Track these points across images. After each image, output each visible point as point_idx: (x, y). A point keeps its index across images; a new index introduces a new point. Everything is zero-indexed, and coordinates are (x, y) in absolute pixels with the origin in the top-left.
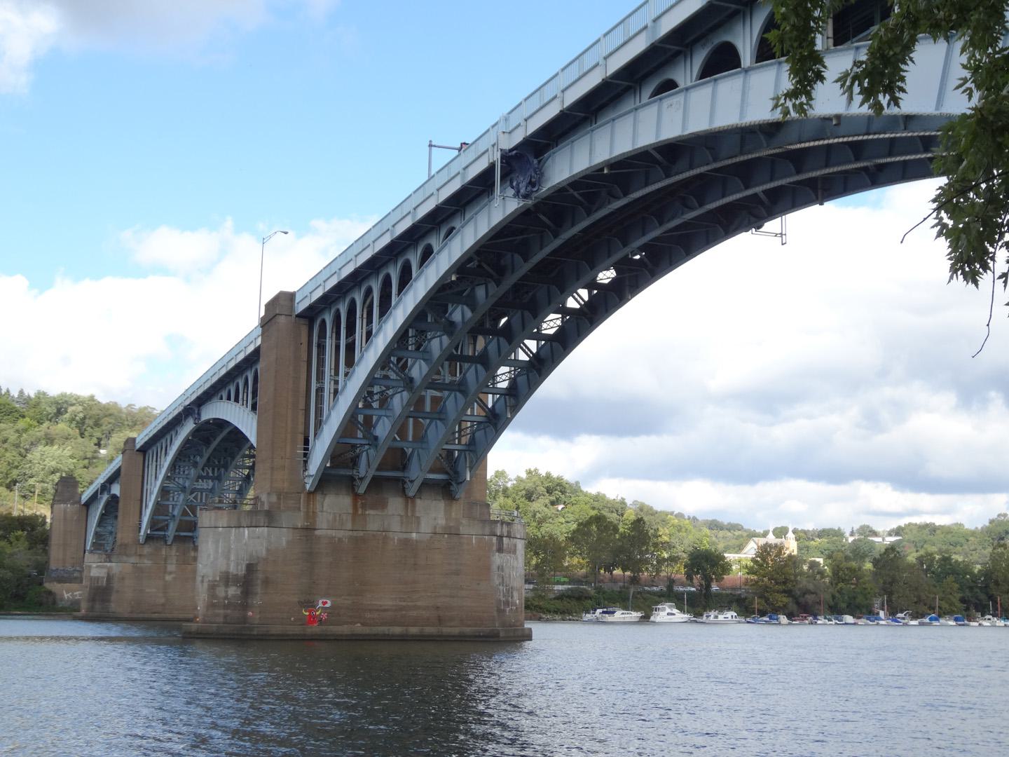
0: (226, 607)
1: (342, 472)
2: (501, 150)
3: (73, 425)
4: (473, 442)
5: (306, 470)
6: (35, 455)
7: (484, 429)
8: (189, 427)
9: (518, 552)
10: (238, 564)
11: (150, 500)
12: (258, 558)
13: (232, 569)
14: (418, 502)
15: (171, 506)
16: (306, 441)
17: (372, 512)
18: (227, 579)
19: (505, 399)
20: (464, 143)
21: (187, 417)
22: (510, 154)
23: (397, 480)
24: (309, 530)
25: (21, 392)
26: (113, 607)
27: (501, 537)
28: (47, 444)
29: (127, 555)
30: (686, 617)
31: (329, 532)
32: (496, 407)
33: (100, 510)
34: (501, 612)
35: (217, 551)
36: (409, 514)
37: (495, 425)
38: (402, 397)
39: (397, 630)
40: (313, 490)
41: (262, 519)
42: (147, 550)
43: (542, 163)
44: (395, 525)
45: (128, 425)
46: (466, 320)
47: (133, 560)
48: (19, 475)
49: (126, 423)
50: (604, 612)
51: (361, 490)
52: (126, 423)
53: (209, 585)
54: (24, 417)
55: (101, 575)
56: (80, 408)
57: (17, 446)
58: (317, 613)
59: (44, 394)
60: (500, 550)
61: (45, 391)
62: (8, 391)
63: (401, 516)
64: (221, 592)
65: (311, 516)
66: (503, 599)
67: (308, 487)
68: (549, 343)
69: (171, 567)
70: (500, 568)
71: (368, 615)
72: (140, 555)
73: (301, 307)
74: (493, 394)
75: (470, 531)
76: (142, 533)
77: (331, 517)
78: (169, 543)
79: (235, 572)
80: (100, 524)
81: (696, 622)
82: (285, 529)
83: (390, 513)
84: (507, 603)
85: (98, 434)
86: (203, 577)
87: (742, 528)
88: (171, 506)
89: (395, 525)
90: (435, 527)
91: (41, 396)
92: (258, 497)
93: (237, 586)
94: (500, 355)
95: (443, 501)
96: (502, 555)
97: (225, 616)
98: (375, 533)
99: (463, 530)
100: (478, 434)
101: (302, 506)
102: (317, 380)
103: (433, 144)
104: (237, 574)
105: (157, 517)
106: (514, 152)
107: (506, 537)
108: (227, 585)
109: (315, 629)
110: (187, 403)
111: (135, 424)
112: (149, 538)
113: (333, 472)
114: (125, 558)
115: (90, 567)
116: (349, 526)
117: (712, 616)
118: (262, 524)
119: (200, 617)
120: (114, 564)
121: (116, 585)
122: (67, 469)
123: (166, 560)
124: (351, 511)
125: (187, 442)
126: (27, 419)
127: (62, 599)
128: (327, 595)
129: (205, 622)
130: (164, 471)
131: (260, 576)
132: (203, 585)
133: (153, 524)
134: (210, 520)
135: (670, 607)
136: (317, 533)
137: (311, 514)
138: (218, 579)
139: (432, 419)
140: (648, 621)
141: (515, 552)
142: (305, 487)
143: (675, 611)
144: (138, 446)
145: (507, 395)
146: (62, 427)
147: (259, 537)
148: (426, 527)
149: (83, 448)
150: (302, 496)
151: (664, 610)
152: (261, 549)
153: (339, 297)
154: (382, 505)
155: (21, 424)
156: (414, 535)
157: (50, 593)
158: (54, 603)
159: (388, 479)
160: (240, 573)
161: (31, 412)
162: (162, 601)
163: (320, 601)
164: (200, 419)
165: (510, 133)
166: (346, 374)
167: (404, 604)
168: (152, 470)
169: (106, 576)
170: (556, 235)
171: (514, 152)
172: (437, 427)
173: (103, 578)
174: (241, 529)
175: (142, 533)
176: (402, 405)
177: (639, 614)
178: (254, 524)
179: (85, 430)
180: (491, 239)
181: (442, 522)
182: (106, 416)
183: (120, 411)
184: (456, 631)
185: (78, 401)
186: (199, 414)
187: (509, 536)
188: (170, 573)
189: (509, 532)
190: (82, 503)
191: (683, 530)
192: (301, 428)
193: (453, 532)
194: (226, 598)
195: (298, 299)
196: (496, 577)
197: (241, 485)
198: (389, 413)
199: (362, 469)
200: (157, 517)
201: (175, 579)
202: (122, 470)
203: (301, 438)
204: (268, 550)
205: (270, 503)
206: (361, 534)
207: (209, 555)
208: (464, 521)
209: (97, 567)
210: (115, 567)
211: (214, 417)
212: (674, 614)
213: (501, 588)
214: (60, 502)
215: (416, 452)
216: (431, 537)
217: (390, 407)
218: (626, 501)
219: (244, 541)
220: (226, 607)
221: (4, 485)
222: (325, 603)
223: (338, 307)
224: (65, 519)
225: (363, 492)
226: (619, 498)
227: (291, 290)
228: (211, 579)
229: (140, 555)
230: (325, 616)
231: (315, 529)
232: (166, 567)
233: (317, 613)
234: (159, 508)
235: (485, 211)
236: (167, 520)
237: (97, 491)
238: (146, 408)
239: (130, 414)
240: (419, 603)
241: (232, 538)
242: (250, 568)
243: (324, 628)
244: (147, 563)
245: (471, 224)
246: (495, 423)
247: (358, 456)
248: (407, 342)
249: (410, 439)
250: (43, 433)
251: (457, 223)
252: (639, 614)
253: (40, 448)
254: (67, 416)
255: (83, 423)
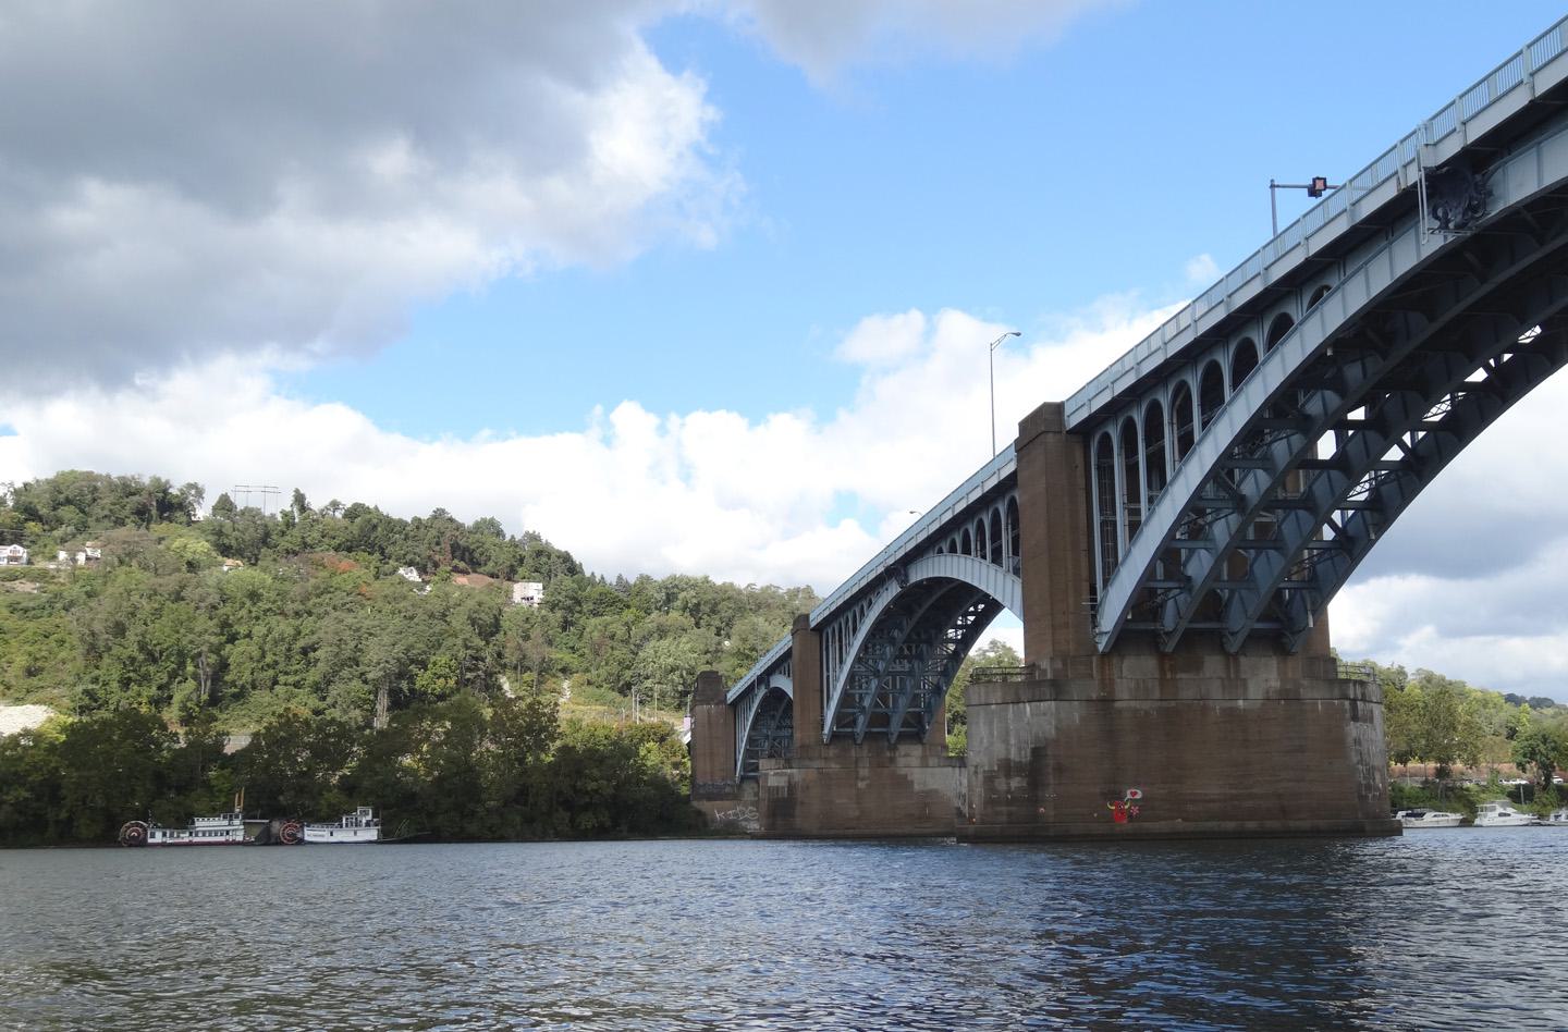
0: (1009, 803)
1: (1142, 626)
2: (1425, 168)
3: (687, 614)
4: (1314, 577)
5: (1095, 626)
6: (648, 651)
7: (1332, 558)
8: (893, 590)
9: (1375, 721)
10: (1020, 749)
11: (835, 688)
12: (1046, 739)
13: (1013, 755)
14: (1243, 660)
15: (857, 696)
16: (1093, 591)
17: (1184, 676)
18: (1008, 768)
19: (1363, 515)
20: (1318, 178)
21: (890, 577)
22: (1439, 172)
23: (1211, 632)
24: (1106, 703)
25: (620, 577)
26: (798, 822)
27: (1354, 701)
28: (661, 638)
29: (810, 759)
30: (1526, 818)
31: (1133, 704)
32: (1348, 528)
33: (754, 710)
34: (1363, 798)
35: (991, 734)
36: (1232, 676)
37: (1350, 553)
38: (1227, 523)
39: (1230, 825)
40: (1107, 650)
41: (1047, 691)
42: (832, 752)
43: (1486, 177)
44: (1216, 691)
45: (751, 609)
46: (1330, 412)
47: (817, 764)
48: (632, 677)
49: (748, 607)
50: (1408, 815)
51: (1169, 649)
52: (748, 607)
53: (985, 777)
54: (628, 607)
55: (782, 784)
56: (693, 593)
57: (626, 642)
58: (1126, 807)
59: (648, 578)
60: (1355, 718)
61: (649, 574)
62: (603, 578)
63: (1222, 679)
64: (1001, 784)
65: (1107, 684)
66: (1363, 782)
67: (1101, 648)
68: (1432, 434)
69: (864, 772)
70: (1357, 742)
71: (1190, 807)
72: (826, 758)
73: (1073, 421)
74: (1342, 509)
75: (1316, 696)
76: (826, 731)
77: (1133, 685)
78: (859, 742)
79: (1017, 759)
80: (753, 727)
81: (1539, 824)
82: (1076, 703)
83: (1208, 675)
84: (1369, 787)
85: (717, 623)
86: (976, 767)
87: (1553, 703)
88: (857, 696)
89: (1216, 691)
90: (1268, 692)
91: (645, 580)
92: (1034, 665)
93: (1021, 776)
94: (1368, 456)
95: (1274, 658)
96: (1358, 724)
97: (1010, 814)
98: (1190, 702)
99: (1305, 693)
100: (1319, 567)
101: (1095, 672)
102: (1101, 510)
103: (1276, 183)
104: (1021, 762)
105: (843, 710)
106: (1445, 169)
107: (1361, 700)
108: (1008, 776)
109: (1125, 826)
110: (891, 561)
111: (760, 608)
112: (834, 736)
113: (1133, 626)
114: (807, 763)
115: (766, 775)
116: (1157, 695)
117: (1564, 816)
118: (1048, 697)
119: (978, 817)
120: (794, 771)
121: (799, 795)
122: (687, 666)
123: (856, 762)
124: (1157, 676)
125: (886, 611)
126: (633, 610)
127: (714, 820)
128: (1137, 784)
129: (983, 823)
130: (853, 651)
131: (1051, 762)
132: (977, 777)
133: (839, 718)
134: (980, 696)
135: (1504, 806)
136: (1118, 705)
137: (1107, 681)
138: (996, 768)
139: (1259, 550)
140: (1471, 826)
141: (1371, 720)
142: (1097, 650)
143: (1510, 810)
144: (813, 624)
145: (1366, 509)
146: (675, 616)
147: (1045, 714)
148: (1256, 690)
149: (704, 640)
150: (1094, 659)
151: (1494, 809)
152: (1049, 730)
153: (1132, 401)
154: (1196, 666)
155: (628, 615)
156: (1241, 703)
157: (699, 813)
158: (705, 824)
159: (1201, 632)
160: (1024, 760)
161: (636, 601)
162: (857, 813)
163: (1129, 792)
164: (908, 581)
165: (1435, 145)
166: (1151, 500)
167: (1234, 791)
168: (833, 653)
169: (787, 784)
170: (1484, 280)
171: (1445, 169)
172: (1268, 558)
173: (783, 788)
174: (1021, 705)
175: (826, 731)
176: (1230, 534)
177: (1459, 816)
178: (1037, 698)
179: (701, 618)
180: (1394, 293)
181: (1275, 684)
182: (724, 600)
183: (739, 592)
184: (1306, 824)
185: (692, 584)
186: (907, 576)
187: (1364, 700)
188: (863, 779)
189: (1363, 694)
190: (729, 702)
191: (1491, 705)
192: (1085, 573)
193: (1289, 696)
194: (1009, 791)
195: (1068, 411)
196: (1353, 754)
197: (946, 665)
198: (1209, 545)
199: (1169, 620)
200: (843, 710)
201: (869, 786)
202: (795, 653)
203: (1085, 586)
204: (1057, 728)
205: (1054, 671)
206: (1173, 704)
207: (982, 739)
208: (1305, 682)
209: (775, 774)
210: (796, 773)
211: (931, 575)
212: (1509, 815)
213: (1360, 767)
214: (702, 702)
215: (1237, 595)
216: (1263, 704)
217: (1210, 537)
218: (1405, 670)
219: (1026, 720)
220: (1009, 803)
221: (616, 689)
222: (1134, 794)
223: (1129, 414)
224: (709, 723)
225: (1171, 650)
226: (1396, 666)
227: (1058, 400)
228: (986, 769)
229: (826, 758)
230: (1135, 810)
231: (1114, 701)
232: (857, 772)
233: (1126, 807)
234: (846, 699)
235: (1384, 256)
236: (855, 713)
237: (753, 683)
238: (768, 587)
239: (751, 595)
240: (1254, 791)
241: (1010, 715)
242: (1037, 752)
243: (1136, 825)
244: (834, 767)
245: (1360, 278)
246: (1349, 552)
247: (1162, 606)
248: (1262, 440)
249: (1226, 578)
250: (655, 624)
251: (1334, 282)
252: (1459, 816)
253: (653, 643)
254: (678, 603)
255: (698, 611)
